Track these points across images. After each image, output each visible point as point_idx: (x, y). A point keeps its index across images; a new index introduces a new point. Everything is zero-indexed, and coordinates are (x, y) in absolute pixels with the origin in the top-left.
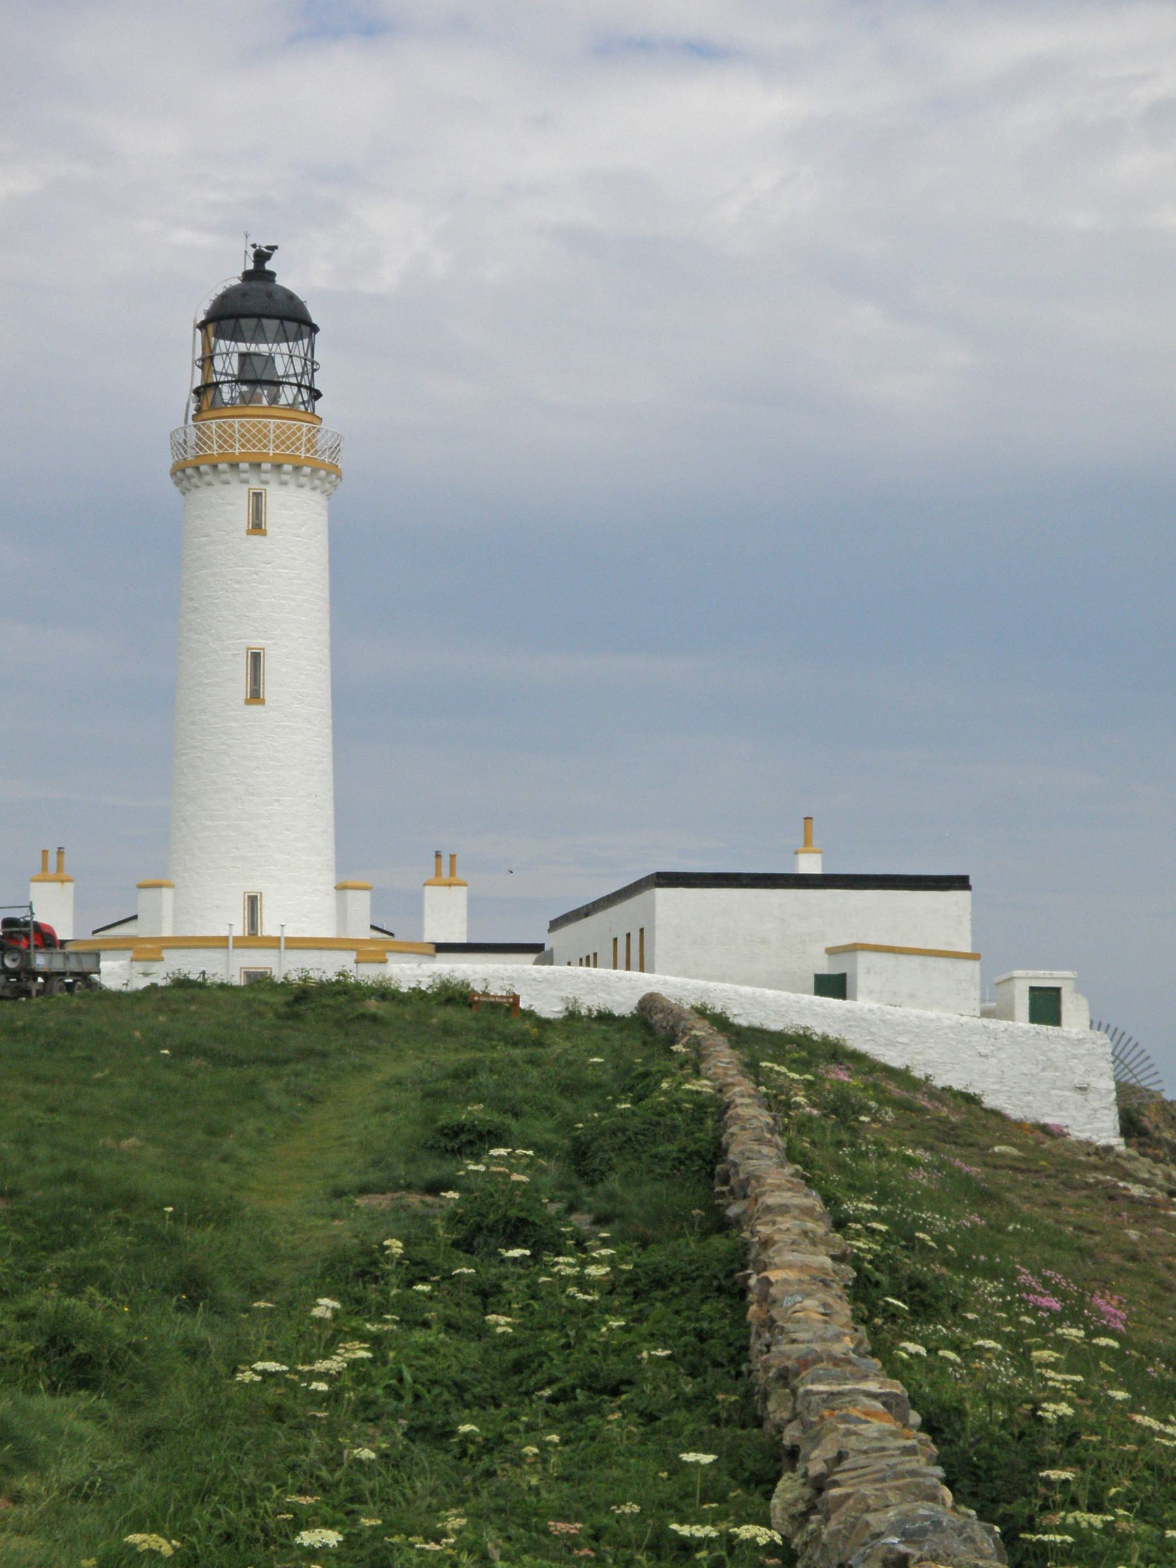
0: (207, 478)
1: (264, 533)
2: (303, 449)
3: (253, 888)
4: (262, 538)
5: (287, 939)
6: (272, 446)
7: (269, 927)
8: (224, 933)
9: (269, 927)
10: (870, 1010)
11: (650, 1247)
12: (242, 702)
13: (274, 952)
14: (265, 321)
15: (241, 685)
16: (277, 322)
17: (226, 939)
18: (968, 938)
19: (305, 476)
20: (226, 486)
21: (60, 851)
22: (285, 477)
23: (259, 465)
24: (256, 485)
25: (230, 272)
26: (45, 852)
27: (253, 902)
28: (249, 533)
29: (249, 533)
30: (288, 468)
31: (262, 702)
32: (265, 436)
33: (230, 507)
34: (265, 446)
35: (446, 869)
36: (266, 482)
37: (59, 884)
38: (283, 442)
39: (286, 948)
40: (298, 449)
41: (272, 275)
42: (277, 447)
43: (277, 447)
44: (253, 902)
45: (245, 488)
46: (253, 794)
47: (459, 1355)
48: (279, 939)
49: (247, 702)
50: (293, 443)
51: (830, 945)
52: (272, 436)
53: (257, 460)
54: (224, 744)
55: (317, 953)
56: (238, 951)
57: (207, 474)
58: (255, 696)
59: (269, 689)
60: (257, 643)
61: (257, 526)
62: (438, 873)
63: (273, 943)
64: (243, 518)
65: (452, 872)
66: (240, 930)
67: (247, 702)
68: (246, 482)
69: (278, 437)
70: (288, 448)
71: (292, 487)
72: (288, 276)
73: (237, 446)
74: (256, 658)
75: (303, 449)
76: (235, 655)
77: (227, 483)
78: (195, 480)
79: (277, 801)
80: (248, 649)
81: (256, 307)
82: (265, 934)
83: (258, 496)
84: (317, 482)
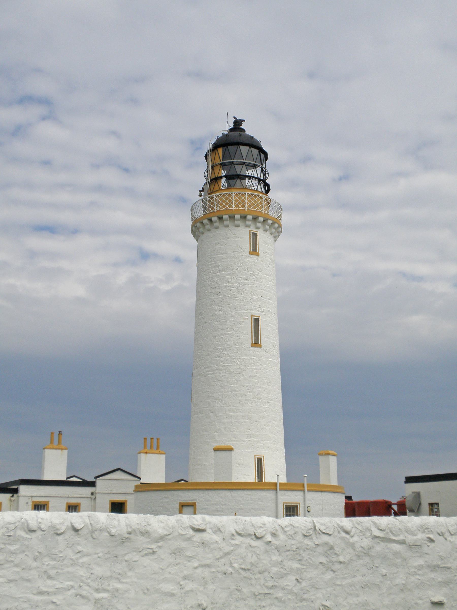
1: (258, 255)
2: (263, 209)
3: (259, 453)
5: (280, 483)
6: (246, 206)
9: (269, 478)
12: (250, 346)
13: (301, 493)
14: (229, 147)
16: (248, 148)
18: (164, 474)
20: (236, 228)
22: (248, 223)
23: (222, 218)
24: (253, 229)
25: (222, 128)
27: (260, 461)
28: (250, 253)
29: (250, 253)
31: (260, 346)
33: (239, 239)
34: (243, 206)
35: (57, 440)
36: (258, 228)
37: (60, 451)
38: (252, 204)
39: (308, 491)
40: (260, 208)
41: (243, 130)
42: (249, 206)
43: (249, 206)
44: (260, 461)
45: (248, 230)
46: (257, 398)
48: (275, 484)
50: (258, 205)
53: (257, 214)
54: (240, 368)
55: (320, 494)
57: (216, 222)
60: (256, 313)
61: (254, 250)
62: (52, 442)
65: (59, 443)
66: (252, 478)
67: (252, 346)
68: (249, 226)
70: (255, 207)
71: (231, 227)
73: (234, 206)
74: (256, 321)
75: (263, 209)
76: (245, 319)
77: (227, 226)
78: (208, 227)
79: (268, 402)
80: (252, 316)
81: (234, 155)
82: (266, 481)
83: (254, 235)
84: (259, 225)
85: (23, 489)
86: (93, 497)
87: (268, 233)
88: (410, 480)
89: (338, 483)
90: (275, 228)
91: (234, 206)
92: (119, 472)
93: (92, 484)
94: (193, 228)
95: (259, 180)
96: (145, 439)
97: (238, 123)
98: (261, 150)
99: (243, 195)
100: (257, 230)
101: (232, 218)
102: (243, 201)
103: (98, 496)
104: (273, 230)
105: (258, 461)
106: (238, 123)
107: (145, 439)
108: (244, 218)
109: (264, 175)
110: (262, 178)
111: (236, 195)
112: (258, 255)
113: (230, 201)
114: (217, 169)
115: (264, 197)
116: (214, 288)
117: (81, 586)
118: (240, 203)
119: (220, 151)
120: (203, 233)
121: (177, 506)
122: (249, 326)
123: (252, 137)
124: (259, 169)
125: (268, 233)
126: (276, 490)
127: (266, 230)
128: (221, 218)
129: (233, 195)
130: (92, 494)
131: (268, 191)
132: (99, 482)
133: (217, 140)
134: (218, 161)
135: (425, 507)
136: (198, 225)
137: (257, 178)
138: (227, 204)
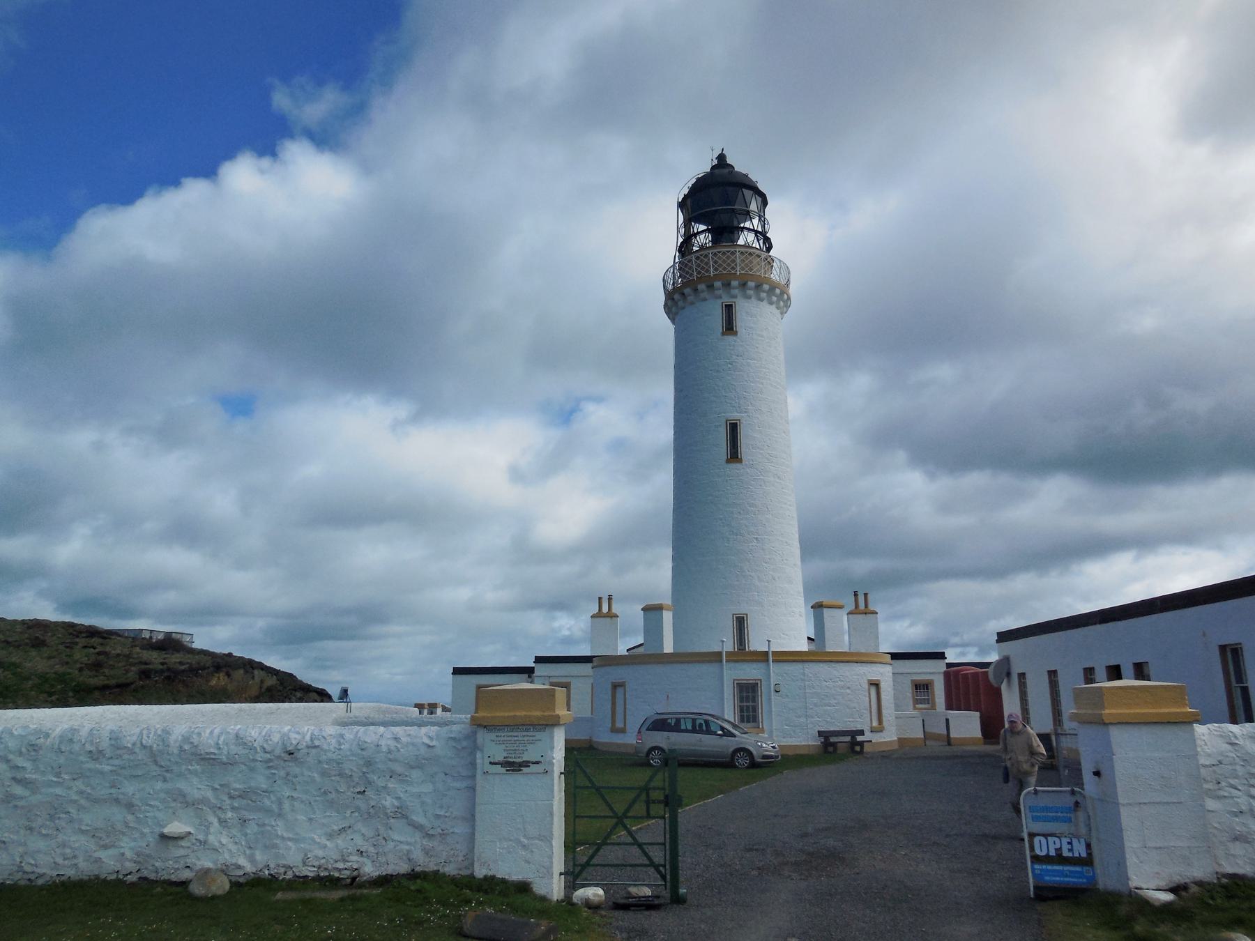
4: (738, 465)
7: (756, 643)
8: (717, 649)
10: (181, 663)
11: (816, 742)
13: (762, 665)
15: (723, 449)
17: (720, 654)
23: (729, 284)
26: (600, 599)
27: (741, 622)
31: (740, 461)
36: (735, 297)
43: (742, 269)
45: (719, 302)
48: (767, 653)
49: (728, 461)
51: (1028, 676)
55: (800, 666)
56: (732, 665)
58: (734, 455)
61: (730, 327)
63: (763, 657)
67: (728, 461)
72: (740, 163)
74: (734, 428)
83: (729, 308)
84: (736, 292)
94: (670, 303)
95: (756, 232)
96: (856, 594)
97: (721, 157)
99: (733, 253)
102: (734, 261)
106: (721, 157)
109: (763, 227)
113: (707, 264)
115: (764, 255)
117: (113, 787)
121: (610, 686)
123: (746, 176)
124: (755, 221)
126: (767, 661)
131: (769, 248)
133: (66, 221)
136: (676, 297)
137: (753, 230)
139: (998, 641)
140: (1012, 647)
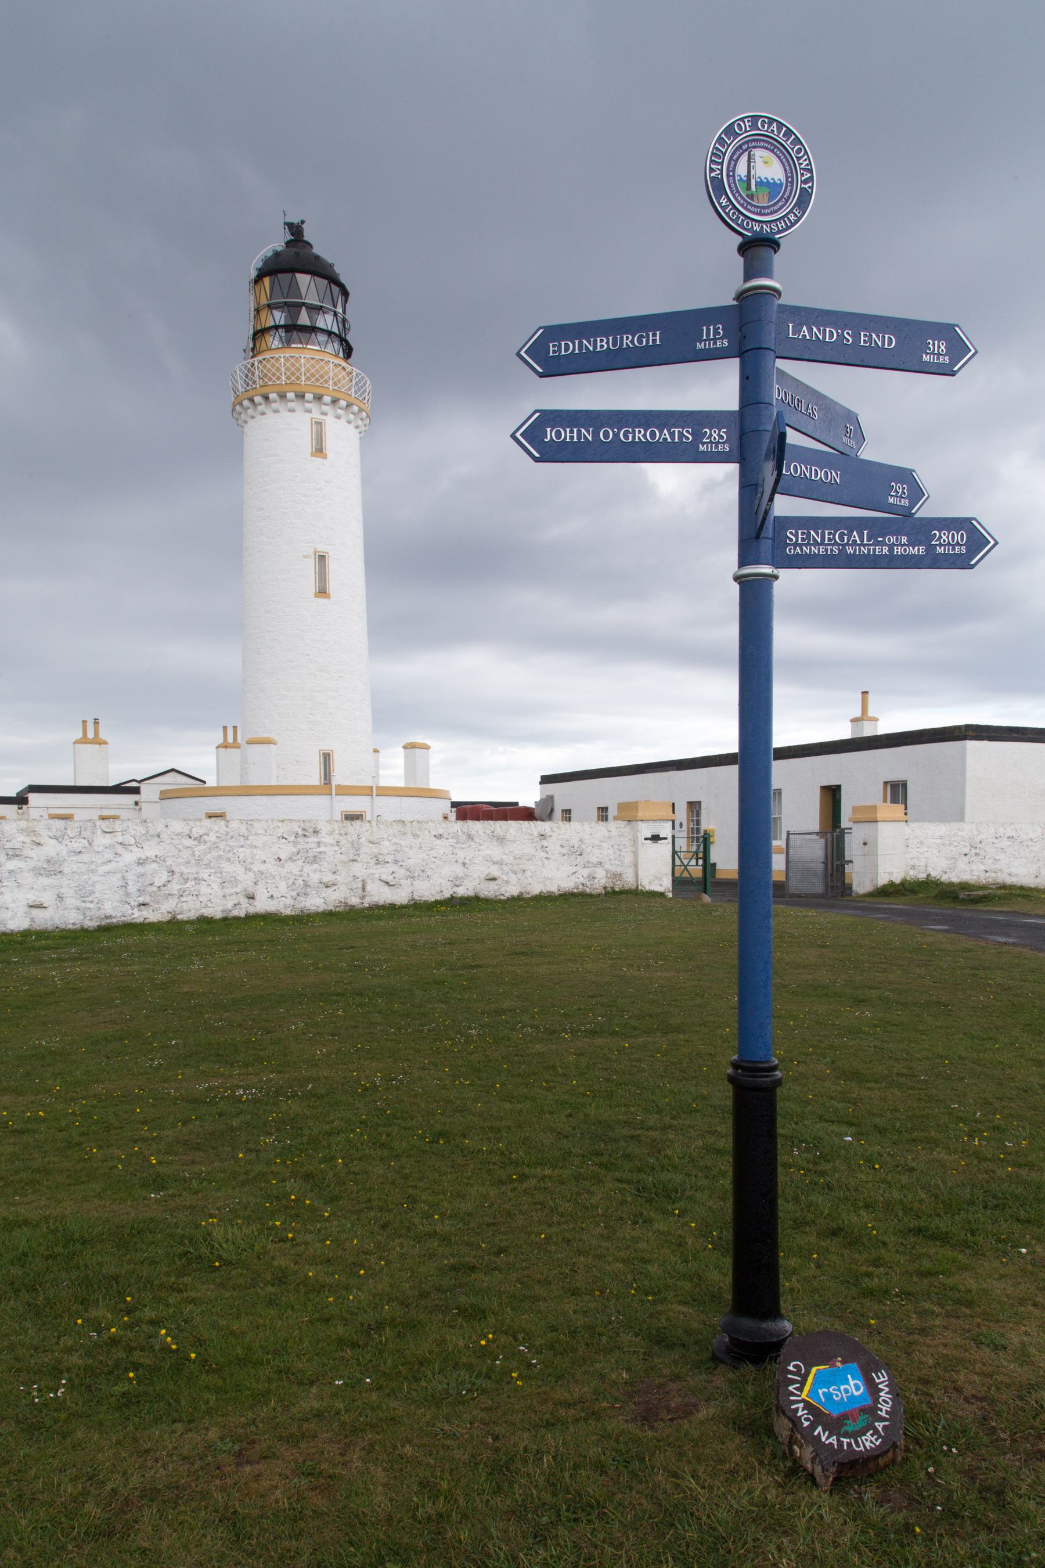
0: (260, 408)
3: (326, 747)
4: (324, 461)
6: (331, 382)
13: (368, 798)
14: (280, 276)
18: (969, 761)
19: (341, 408)
21: (96, 722)
23: (303, 396)
24: (316, 415)
26: (84, 722)
27: (327, 758)
28: (313, 455)
29: (313, 455)
30: (291, 395)
31: (328, 597)
32: (298, 370)
36: (325, 414)
37: (97, 746)
42: (308, 379)
44: (327, 758)
45: (308, 416)
47: (898, 1115)
52: (303, 370)
55: (397, 799)
57: (260, 404)
58: (322, 592)
59: (332, 587)
60: (322, 548)
61: (319, 450)
64: (307, 443)
66: (314, 778)
68: (310, 411)
69: (308, 370)
70: (317, 380)
71: (259, 417)
73: (283, 378)
74: (322, 558)
77: (292, 411)
80: (315, 552)
81: (293, 259)
83: (319, 424)
85: (32, 797)
86: (137, 808)
87: (343, 421)
88: (546, 780)
89: (406, 781)
90: (353, 413)
91: (283, 378)
92: (171, 774)
93: (136, 791)
96: (225, 728)
98: (333, 280)
100: (323, 417)
101: (282, 396)
103: (143, 805)
104: (352, 417)
105: (325, 758)
106: (296, 230)
107: (225, 728)
108: (300, 396)
110: (335, 330)
111: (287, 359)
112: (325, 457)
114: (263, 314)
116: (262, 509)
118: (293, 374)
119: (267, 281)
120: (246, 422)
122: (310, 567)
125: (343, 421)
127: (338, 417)
128: (266, 398)
129: (282, 360)
130: (136, 803)
132: (143, 787)
134: (264, 301)
135: (558, 813)
138: (274, 375)
139: (541, 783)
140: (552, 788)
